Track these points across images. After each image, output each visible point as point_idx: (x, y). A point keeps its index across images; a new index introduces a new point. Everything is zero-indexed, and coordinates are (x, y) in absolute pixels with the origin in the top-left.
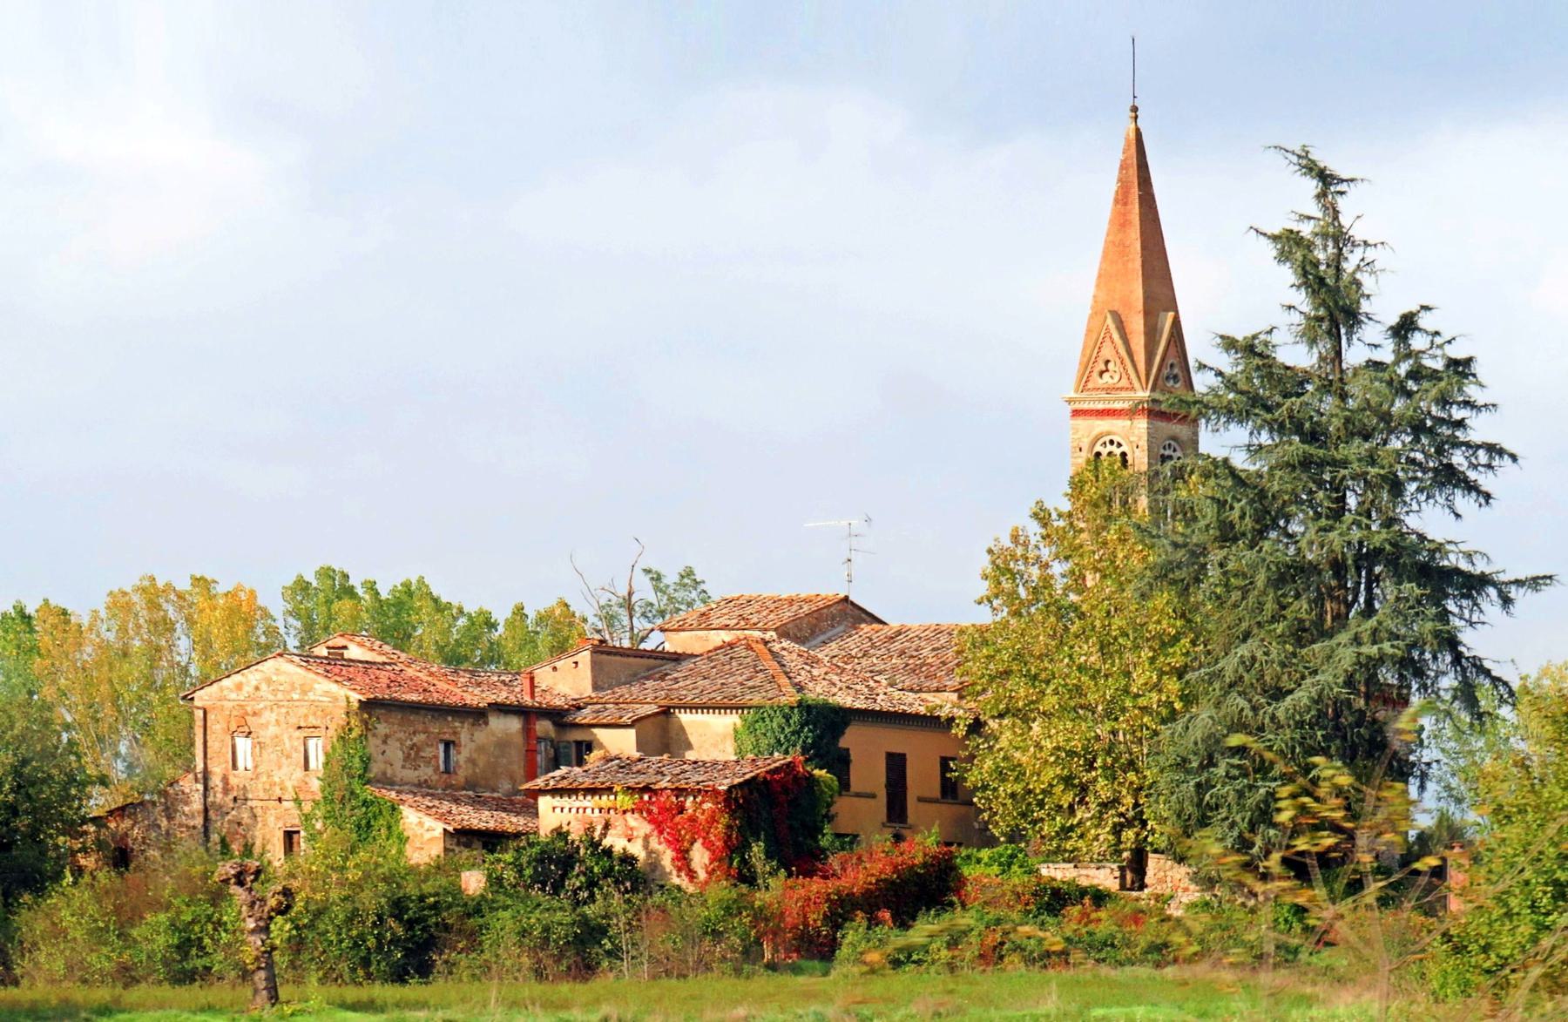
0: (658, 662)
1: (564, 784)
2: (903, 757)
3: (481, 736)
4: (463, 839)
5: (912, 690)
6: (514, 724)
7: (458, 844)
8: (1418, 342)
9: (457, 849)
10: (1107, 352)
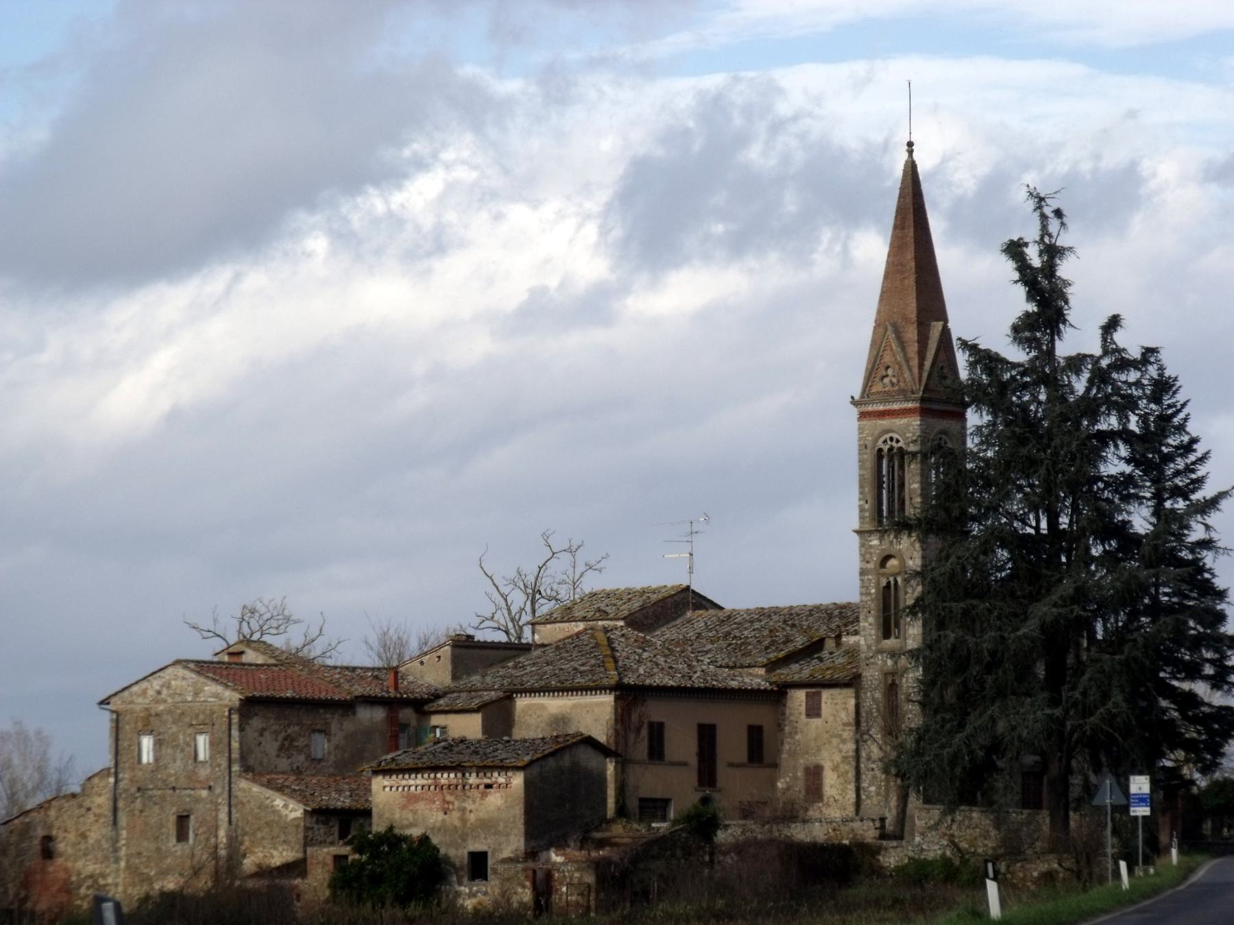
0: (515, 653)
1: (393, 766)
2: (661, 725)
3: (349, 726)
4: (322, 818)
5: (727, 667)
6: (379, 714)
7: (317, 822)
8: (1120, 338)
9: (316, 827)
10: (887, 359)
